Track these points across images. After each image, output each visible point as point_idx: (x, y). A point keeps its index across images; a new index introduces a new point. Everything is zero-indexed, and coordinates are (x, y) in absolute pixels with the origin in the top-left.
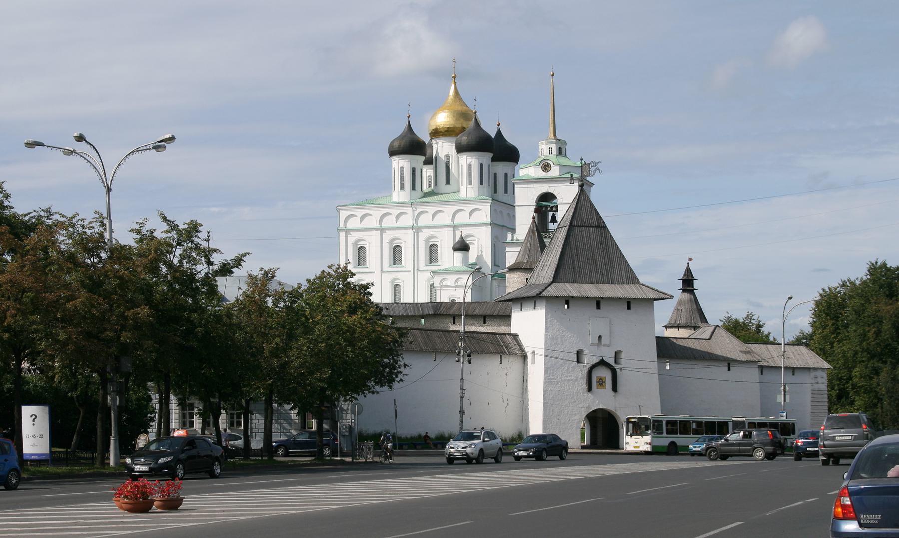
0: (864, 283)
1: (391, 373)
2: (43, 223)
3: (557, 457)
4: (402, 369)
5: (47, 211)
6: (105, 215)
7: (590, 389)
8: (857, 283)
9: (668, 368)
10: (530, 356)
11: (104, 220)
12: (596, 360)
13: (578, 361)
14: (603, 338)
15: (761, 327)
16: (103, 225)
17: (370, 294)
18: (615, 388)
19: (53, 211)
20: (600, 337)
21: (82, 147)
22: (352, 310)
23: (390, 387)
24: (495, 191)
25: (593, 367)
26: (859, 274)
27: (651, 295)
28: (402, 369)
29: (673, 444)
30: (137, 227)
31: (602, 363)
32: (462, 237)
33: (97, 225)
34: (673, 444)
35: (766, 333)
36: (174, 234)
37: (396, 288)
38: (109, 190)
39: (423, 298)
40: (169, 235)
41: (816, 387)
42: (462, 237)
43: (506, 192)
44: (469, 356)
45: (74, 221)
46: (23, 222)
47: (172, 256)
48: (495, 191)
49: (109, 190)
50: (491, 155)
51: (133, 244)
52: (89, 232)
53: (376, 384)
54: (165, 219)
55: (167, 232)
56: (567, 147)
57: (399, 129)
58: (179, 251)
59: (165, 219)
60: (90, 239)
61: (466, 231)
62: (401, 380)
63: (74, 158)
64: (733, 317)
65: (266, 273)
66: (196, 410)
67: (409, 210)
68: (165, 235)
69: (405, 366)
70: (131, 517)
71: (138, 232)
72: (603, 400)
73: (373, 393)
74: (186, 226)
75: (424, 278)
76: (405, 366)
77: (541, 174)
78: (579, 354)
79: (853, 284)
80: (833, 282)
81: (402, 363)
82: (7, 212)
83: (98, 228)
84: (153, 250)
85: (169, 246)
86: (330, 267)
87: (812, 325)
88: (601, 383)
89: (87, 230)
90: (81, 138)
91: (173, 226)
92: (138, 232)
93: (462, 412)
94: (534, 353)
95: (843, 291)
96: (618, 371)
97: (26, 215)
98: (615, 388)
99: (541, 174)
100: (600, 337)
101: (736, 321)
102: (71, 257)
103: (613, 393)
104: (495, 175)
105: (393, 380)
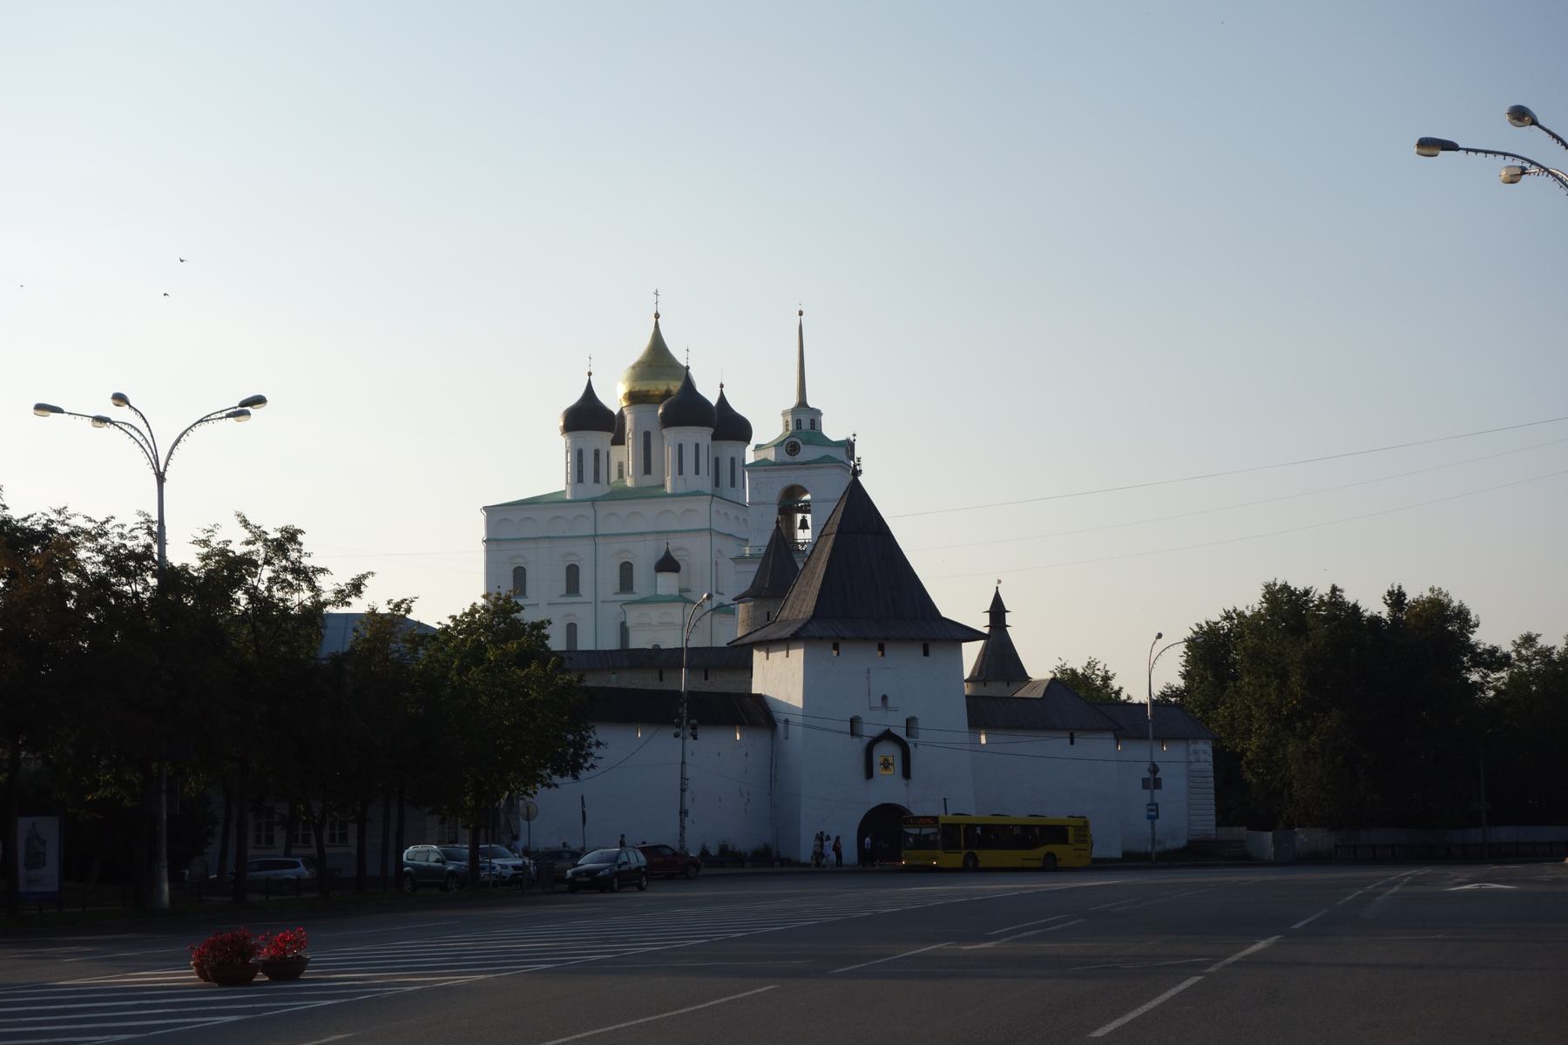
1: (576, 755)
2: (53, 531)
4: (594, 749)
5: (59, 513)
6: (155, 517)
7: (869, 774)
8: (1248, 613)
9: (983, 740)
10: (781, 726)
13: (853, 734)
14: (890, 700)
16: (150, 533)
17: (547, 637)
18: (906, 773)
19: (70, 511)
20: (884, 698)
22: (523, 659)
23: (576, 777)
24: (717, 484)
25: (875, 741)
26: (1250, 600)
28: (594, 749)
29: (1050, 855)
30: (203, 537)
31: (888, 736)
32: (668, 552)
34: (1050, 855)
37: (572, 630)
38: (161, 478)
39: (610, 643)
40: (252, 548)
41: (1196, 766)
42: (668, 552)
44: (694, 728)
45: (108, 527)
46: (22, 530)
47: (255, 581)
48: (717, 484)
49: (161, 478)
50: (710, 431)
51: (194, 563)
52: (129, 544)
54: (246, 523)
55: (248, 543)
56: (824, 419)
57: (574, 396)
58: (266, 572)
59: (246, 523)
60: (132, 555)
61: (675, 544)
63: (108, 430)
65: (398, 606)
68: (246, 549)
69: (598, 744)
70: (224, 994)
71: (205, 543)
72: (888, 788)
73: (549, 786)
74: (278, 535)
76: (598, 744)
77: (788, 458)
78: (854, 722)
79: (1241, 615)
80: (1213, 613)
83: (144, 539)
84: (229, 570)
89: (126, 542)
90: (120, 399)
91: (259, 535)
92: (205, 543)
95: (1226, 624)
96: (911, 746)
97: (25, 520)
98: (906, 773)
99: (788, 458)
100: (884, 698)
101: (1073, 672)
102: (101, 582)
103: (904, 781)
104: (717, 460)
105: (581, 767)
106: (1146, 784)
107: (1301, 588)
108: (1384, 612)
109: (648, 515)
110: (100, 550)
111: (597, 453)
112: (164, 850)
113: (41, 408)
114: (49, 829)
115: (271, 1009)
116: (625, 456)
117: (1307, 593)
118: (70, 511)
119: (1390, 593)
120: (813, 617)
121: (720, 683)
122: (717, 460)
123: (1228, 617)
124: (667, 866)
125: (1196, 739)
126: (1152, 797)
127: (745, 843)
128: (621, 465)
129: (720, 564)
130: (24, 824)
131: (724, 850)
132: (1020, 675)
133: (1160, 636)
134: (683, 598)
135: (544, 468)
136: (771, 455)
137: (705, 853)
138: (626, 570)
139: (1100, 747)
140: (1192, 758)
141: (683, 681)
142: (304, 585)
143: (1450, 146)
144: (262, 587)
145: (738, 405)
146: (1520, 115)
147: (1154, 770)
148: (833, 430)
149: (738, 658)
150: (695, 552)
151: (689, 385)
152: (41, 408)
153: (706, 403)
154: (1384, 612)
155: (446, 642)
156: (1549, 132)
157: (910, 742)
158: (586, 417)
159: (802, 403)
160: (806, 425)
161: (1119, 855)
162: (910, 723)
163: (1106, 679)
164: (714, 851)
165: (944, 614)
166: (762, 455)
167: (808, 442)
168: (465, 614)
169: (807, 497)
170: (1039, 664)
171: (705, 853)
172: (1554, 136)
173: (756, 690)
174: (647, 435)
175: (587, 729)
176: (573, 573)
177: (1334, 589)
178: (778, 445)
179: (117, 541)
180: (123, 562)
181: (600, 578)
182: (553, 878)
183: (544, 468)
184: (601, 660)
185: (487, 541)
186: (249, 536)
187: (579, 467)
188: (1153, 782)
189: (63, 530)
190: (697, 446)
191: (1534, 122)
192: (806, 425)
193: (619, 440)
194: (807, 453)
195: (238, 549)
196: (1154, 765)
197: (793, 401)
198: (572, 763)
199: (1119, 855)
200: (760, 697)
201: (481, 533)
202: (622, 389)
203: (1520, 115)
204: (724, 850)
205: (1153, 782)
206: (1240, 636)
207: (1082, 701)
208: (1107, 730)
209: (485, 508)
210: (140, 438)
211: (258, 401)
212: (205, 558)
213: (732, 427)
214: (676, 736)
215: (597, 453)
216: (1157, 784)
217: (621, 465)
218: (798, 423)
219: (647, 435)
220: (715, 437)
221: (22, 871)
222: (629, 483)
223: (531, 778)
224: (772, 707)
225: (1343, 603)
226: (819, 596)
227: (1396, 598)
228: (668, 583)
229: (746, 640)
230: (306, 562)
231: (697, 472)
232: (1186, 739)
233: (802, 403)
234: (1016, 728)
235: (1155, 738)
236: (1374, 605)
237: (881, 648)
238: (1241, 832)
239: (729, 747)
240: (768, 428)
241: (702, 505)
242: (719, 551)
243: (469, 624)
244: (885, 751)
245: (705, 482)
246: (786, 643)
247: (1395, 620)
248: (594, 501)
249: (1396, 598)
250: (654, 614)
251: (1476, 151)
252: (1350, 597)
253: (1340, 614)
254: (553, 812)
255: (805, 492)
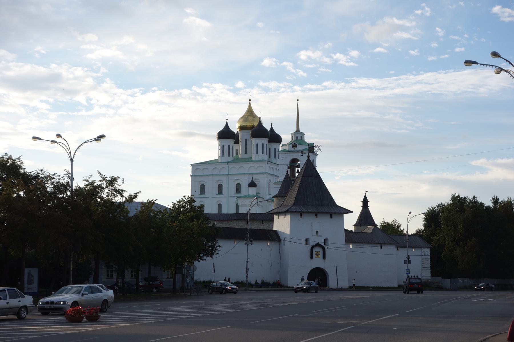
0: (448, 205)
1: (212, 250)
2: (39, 176)
3: (416, 292)
4: (218, 248)
6: (70, 172)
7: (312, 257)
8: (446, 205)
9: (351, 246)
10: (282, 241)
11: (71, 177)
12: (315, 243)
13: (306, 244)
14: (319, 234)
15: (400, 226)
16: (69, 177)
18: (324, 257)
19: (45, 170)
20: (317, 232)
21: (59, 140)
23: (212, 257)
24: (270, 157)
27: (342, 212)
28: (218, 248)
30: (87, 179)
31: (318, 245)
32: (252, 180)
33: (66, 178)
35: (402, 229)
36: (104, 182)
37: (220, 206)
38: (72, 161)
39: (233, 211)
40: (102, 183)
41: (424, 257)
42: (252, 180)
43: (275, 158)
44: (251, 241)
45: (55, 176)
48: (270, 157)
49: (72, 161)
50: (268, 139)
52: (61, 181)
53: (205, 255)
55: (101, 181)
56: (305, 136)
57: (221, 128)
58: (106, 191)
60: (62, 185)
61: (255, 177)
62: (217, 254)
64: (386, 221)
66: (114, 269)
67: (226, 166)
69: (219, 246)
71: (87, 181)
72: (318, 262)
73: (203, 260)
75: (233, 201)
76: (219, 246)
77: (293, 149)
78: (307, 240)
80: (434, 204)
81: (218, 245)
82: (22, 171)
83: (67, 180)
84: (93, 190)
85: (100, 187)
86: (184, 197)
87: (425, 226)
88: (317, 254)
90: (59, 136)
91: (104, 179)
92: (87, 181)
93: (247, 269)
94: (284, 240)
95: (439, 209)
96: (326, 249)
97: (31, 172)
98: (324, 257)
99: (293, 149)
100: (317, 232)
101: (388, 223)
104: (270, 149)
106: (405, 262)
107: (463, 197)
108: (492, 205)
109: (246, 168)
110: (52, 184)
111: (229, 147)
112: (72, 279)
113: (35, 138)
114: (35, 272)
115: (79, 330)
116: (240, 147)
117: (465, 198)
118: (45, 170)
119: (493, 199)
120: (294, 205)
121: (265, 226)
122: (270, 149)
123: (439, 206)
124: (243, 286)
125: (424, 248)
126: (408, 267)
127: (270, 279)
128: (237, 150)
129: (270, 184)
130: (27, 271)
131: (263, 282)
132: (372, 222)
133: (410, 213)
134: (258, 196)
135: (210, 151)
136: (287, 148)
137: (256, 283)
138: (238, 186)
139: (391, 250)
140: (423, 254)
141: (249, 226)
142: (119, 195)
143: (475, 63)
144: (105, 196)
145: (277, 131)
146: (495, 54)
147: (408, 257)
148: (308, 139)
149: (268, 217)
150: (262, 181)
151: (260, 124)
152: (35, 138)
153: (265, 130)
154: (492, 205)
155: (165, 213)
156: (505, 59)
157: (325, 247)
158: (226, 134)
159: (298, 131)
160: (299, 138)
161: (397, 286)
162: (326, 240)
163: (399, 226)
164: (259, 282)
165: (338, 204)
166: (284, 148)
167: (300, 144)
168: (178, 202)
169: (299, 162)
170: (379, 219)
171: (256, 283)
172: (507, 60)
173: (274, 229)
174: (246, 140)
175: (216, 241)
176: (220, 187)
177: (474, 197)
178: (289, 144)
179: (58, 180)
180: (60, 188)
181: (229, 188)
182: (209, 289)
183: (210, 151)
184: (229, 217)
185: (192, 176)
186: (101, 179)
187: (223, 151)
188: (408, 262)
189: (43, 176)
190: (263, 144)
191: (499, 56)
192: (299, 138)
193: (237, 142)
194: (299, 148)
195: (98, 183)
196: (408, 256)
197: (294, 130)
198: (210, 252)
199: (397, 286)
200: (276, 231)
201: (190, 173)
202: (238, 125)
203: (495, 54)
204: (263, 282)
205: (408, 262)
206: (443, 212)
207: (391, 233)
208: (393, 244)
209: (191, 165)
210: (65, 148)
211: (103, 136)
212: (87, 186)
213: (274, 138)
214: (245, 244)
215: (229, 147)
216: (409, 262)
217: (237, 150)
218: (297, 137)
219: (246, 140)
220: (269, 142)
221: (26, 285)
222: (240, 156)
223: (199, 258)
224: (279, 234)
225: (477, 202)
226: (296, 198)
227: (495, 200)
228: (252, 191)
229: (271, 212)
230: (119, 188)
231: (263, 153)
232: (421, 247)
233: (298, 131)
234: (362, 243)
235: (410, 247)
236: (488, 203)
237: (316, 215)
238: (439, 279)
239: (261, 250)
240: (286, 138)
241: (264, 165)
242: (270, 180)
243: (178, 207)
244: (317, 250)
245: (265, 157)
246: (285, 213)
247: (495, 208)
248: (228, 163)
249: (495, 200)
250: (248, 201)
251: (484, 65)
252: (479, 200)
253: (476, 206)
254: (203, 269)
255: (299, 161)
